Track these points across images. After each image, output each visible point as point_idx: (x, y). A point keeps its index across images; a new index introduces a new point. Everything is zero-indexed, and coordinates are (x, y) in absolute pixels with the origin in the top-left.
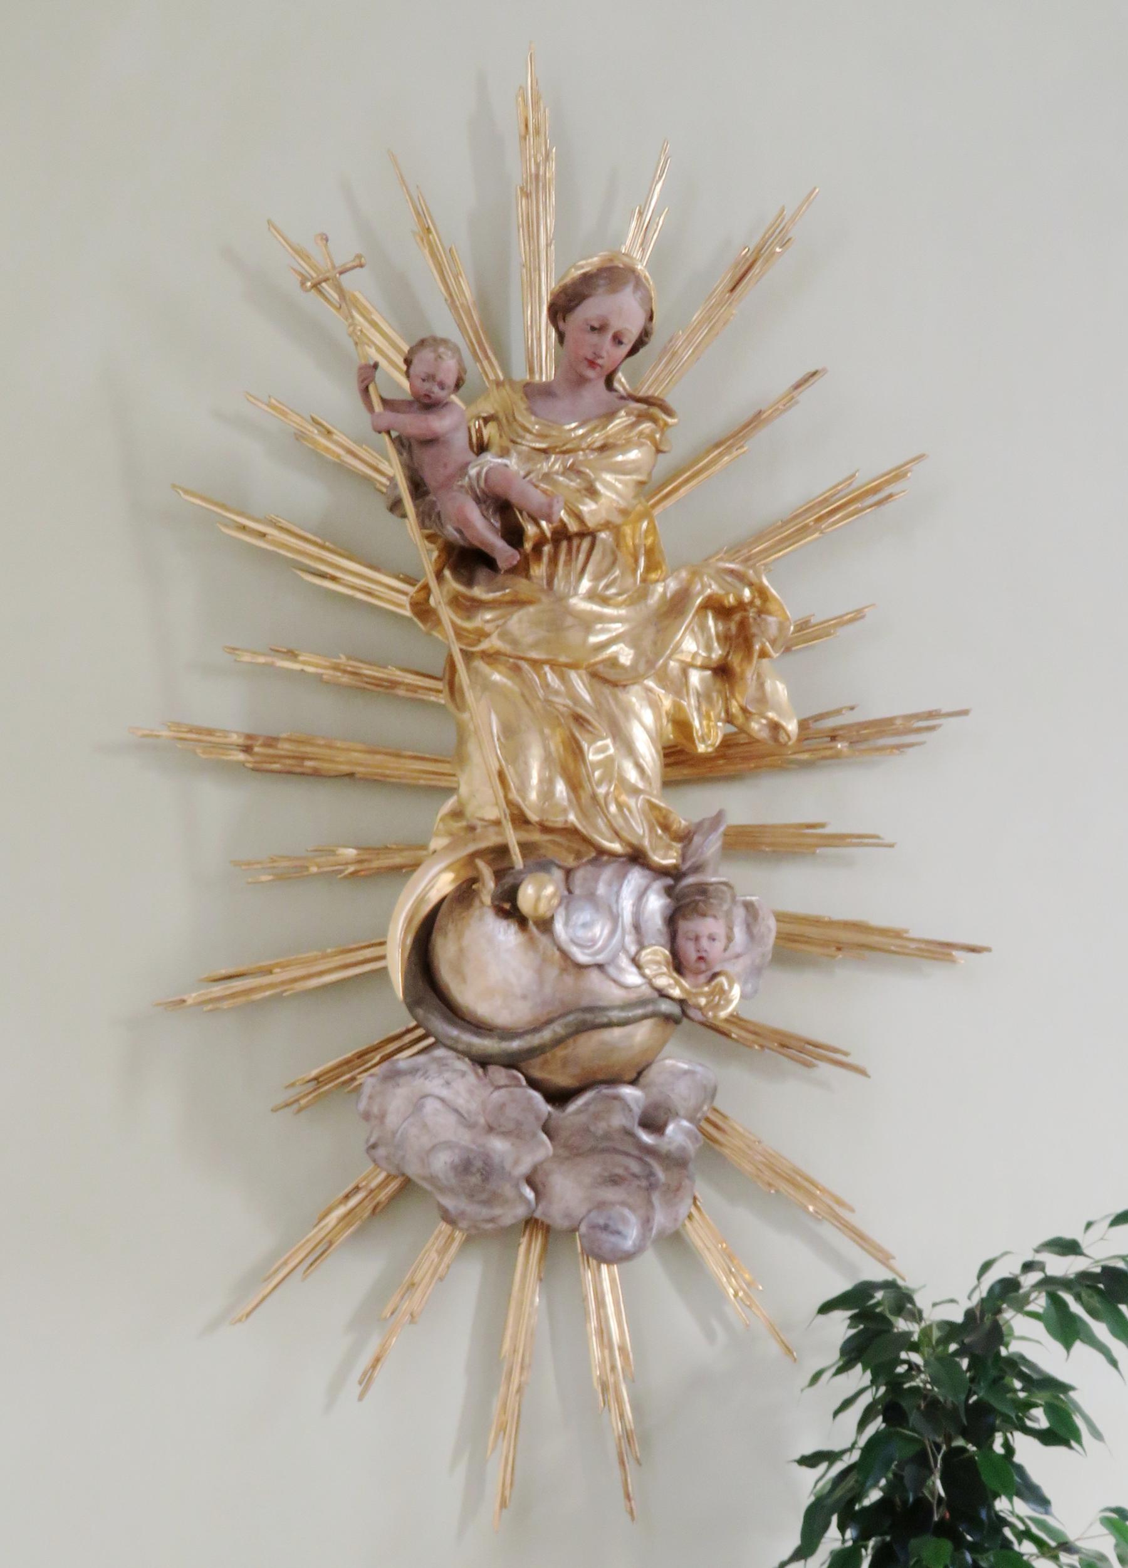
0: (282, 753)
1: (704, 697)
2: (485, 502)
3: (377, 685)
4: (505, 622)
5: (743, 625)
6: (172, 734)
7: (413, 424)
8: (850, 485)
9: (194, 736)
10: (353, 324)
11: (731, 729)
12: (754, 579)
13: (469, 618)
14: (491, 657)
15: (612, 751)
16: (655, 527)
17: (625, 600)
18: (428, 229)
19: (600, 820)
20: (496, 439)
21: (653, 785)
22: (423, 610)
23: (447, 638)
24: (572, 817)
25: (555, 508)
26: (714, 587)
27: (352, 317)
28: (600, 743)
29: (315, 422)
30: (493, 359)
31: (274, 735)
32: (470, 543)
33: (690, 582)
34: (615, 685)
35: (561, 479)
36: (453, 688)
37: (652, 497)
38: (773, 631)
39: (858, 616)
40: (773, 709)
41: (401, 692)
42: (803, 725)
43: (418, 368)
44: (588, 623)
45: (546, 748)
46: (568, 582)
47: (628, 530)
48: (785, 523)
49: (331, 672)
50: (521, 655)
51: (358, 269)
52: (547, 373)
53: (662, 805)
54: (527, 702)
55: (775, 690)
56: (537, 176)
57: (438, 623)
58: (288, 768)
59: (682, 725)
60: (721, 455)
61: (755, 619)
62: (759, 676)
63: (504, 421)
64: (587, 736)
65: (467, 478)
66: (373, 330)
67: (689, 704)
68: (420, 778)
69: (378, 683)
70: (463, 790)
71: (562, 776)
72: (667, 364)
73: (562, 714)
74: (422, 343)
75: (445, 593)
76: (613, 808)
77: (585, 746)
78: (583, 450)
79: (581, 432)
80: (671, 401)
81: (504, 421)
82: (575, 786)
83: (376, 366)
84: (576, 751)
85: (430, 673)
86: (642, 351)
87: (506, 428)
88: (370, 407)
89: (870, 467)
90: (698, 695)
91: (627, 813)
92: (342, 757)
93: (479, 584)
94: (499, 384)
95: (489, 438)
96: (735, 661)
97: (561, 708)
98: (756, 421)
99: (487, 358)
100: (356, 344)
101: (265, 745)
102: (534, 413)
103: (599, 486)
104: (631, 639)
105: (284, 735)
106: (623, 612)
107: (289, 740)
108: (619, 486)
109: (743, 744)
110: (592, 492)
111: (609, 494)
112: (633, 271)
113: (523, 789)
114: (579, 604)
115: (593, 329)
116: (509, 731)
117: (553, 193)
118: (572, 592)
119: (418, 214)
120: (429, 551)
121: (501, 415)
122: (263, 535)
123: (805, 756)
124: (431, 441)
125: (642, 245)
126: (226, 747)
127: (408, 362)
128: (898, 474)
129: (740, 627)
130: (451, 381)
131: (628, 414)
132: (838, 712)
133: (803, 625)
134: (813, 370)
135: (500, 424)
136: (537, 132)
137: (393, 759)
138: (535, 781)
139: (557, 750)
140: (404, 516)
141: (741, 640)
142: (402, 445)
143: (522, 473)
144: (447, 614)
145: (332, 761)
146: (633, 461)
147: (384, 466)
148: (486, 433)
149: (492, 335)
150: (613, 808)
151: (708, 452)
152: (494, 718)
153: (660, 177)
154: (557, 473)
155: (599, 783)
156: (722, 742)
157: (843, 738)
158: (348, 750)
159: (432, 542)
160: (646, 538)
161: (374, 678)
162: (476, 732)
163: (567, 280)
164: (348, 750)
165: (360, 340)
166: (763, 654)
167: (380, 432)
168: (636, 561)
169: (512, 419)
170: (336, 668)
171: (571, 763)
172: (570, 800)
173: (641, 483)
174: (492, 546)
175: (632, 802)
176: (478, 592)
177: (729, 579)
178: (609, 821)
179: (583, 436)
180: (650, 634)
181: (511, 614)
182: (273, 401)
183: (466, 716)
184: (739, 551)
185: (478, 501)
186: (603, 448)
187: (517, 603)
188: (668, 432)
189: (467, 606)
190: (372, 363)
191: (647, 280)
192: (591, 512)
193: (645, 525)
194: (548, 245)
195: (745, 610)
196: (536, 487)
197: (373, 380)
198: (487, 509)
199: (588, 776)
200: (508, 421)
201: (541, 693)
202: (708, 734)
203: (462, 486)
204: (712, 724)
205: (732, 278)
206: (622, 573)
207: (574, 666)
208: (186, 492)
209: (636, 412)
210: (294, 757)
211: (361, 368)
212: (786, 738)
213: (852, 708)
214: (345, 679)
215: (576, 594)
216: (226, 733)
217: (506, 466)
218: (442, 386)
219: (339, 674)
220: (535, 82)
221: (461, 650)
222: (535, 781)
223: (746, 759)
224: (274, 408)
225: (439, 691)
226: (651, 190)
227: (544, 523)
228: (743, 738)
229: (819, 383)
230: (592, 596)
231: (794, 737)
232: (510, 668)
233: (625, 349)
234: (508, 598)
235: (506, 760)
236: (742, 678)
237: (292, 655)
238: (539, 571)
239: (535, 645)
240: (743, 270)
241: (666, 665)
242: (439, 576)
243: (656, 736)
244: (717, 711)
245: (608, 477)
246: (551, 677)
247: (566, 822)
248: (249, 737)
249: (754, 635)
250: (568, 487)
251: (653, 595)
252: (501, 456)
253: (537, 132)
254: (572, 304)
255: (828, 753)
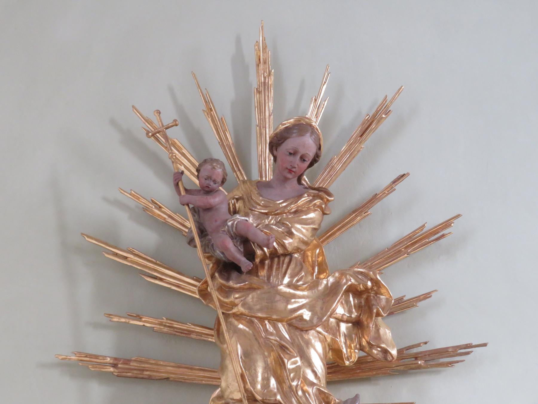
0: (132, 367)
1: (348, 336)
2: (236, 239)
3: (182, 333)
4: (245, 299)
5: (367, 300)
6: (77, 358)
7: (200, 200)
8: (422, 230)
9: (88, 359)
10: (172, 153)
11: (363, 354)
12: (373, 277)
13: (227, 297)
14: (239, 317)
15: (299, 363)
16: (323, 252)
17: (307, 287)
18: (211, 109)
19: (293, 399)
20: (242, 208)
21: (322, 382)
22: (204, 294)
23: (216, 307)
24: (279, 397)
25: (271, 241)
26: (353, 281)
27: (171, 150)
28: (293, 360)
29: (153, 202)
30: (243, 172)
31: (128, 358)
32: (228, 259)
33: (340, 278)
34: (302, 330)
35: (274, 227)
36: (219, 333)
37: (322, 237)
38: (383, 303)
39: (427, 296)
40: (383, 343)
41: (193, 336)
42: (400, 351)
43: (203, 173)
44: (288, 298)
45: (266, 362)
46: (278, 278)
47: (309, 254)
48: (389, 249)
49: (158, 326)
50: (253, 315)
51: (175, 127)
52: (269, 176)
53: (326, 391)
54: (256, 339)
55: (386, 333)
56: (265, 82)
57: (212, 300)
58: (135, 375)
59: (337, 352)
60: (356, 216)
61: (374, 297)
62: (376, 326)
63: (246, 200)
64: (286, 356)
65: (226, 227)
66: (183, 158)
67: (340, 341)
68: (202, 380)
69: (182, 331)
70: (223, 384)
71: (274, 377)
72: (329, 172)
73: (274, 344)
74: (205, 161)
75: (215, 285)
76: (300, 393)
77: (286, 361)
78: (286, 213)
79: (284, 204)
80: (331, 189)
81: (246, 200)
82: (280, 382)
83: (182, 173)
84: (282, 365)
85: (208, 327)
86: (316, 165)
87: (247, 204)
88: (179, 193)
89: (433, 220)
90: (345, 336)
91: (307, 396)
92: (163, 369)
93: (232, 280)
94: (244, 182)
95: (239, 208)
96: (364, 318)
97: (273, 341)
98: (374, 199)
99: (239, 170)
100: (173, 162)
101: (124, 363)
102: (261, 196)
103: (293, 231)
104: (311, 307)
105: (133, 359)
106: (305, 293)
107: (135, 361)
108: (304, 231)
109: (370, 362)
110: (290, 234)
111: (298, 234)
112: (311, 125)
113: (254, 383)
114: (283, 288)
115: (290, 154)
116: (247, 355)
117: (272, 91)
118: (280, 283)
119: (206, 102)
120: (208, 265)
121: (245, 197)
122: (126, 258)
123: (402, 368)
124: (209, 209)
125: (316, 115)
126: (105, 364)
127: (198, 170)
128: (447, 224)
129: (366, 301)
130: (219, 180)
131: (308, 196)
132: (418, 345)
133: (399, 301)
134: (402, 174)
135: (244, 202)
136: (265, 63)
137: (189, 371)
138: (260, 379)
139: (271, 363)
140: (195, 246)
141: (367, 307)
142: (195, 211)
143: (255, 225)
144: (215, 295)
145: (157, 372)
146: (311, 219)
147: (187, 224)
148: (237, 205)
149: (241, 157)
150: (300, 393)
151: (350, 215)
152: (239, 346)
153: (325, 83)
154: (272, 224)
155: (293, 380)
156: (357, 361)
157: (421, 358)
158: (166, 366)
159: (210, 260)
160: (318, 257)
161: (180, 329)
162: (230, 355)
163: (278, 130)
164: (166, 366)
165: (175, 161)
166: (378, 314)
167: (184, 205)
168: (313, 269)
169: (250, 198)
170: (161, 324)
171: (278, 369)
172: (278, 389)
173: (315, 229)
174: (239, 260)
175: (310, 390)
176: (231, 283)
177: (360, 277)
178: (298, 399)
179: (285, 207)
180: (319, 304)
181: (249, 295)
182: (133, 192)
183: (225, 346)
184: (366, 264)
185: (232, 238)
186: (296, 212)
187: (251, 289)
188: (330, 204)
189: (226, 291)
190: (180, 171)
191: (317, 130)
192: (289, 243)
193: (318, 251)
194: (270, 116)
195: (369, 293)
196: (262, 231)
197: (181, 180)
198: (237, 242)
199: (287, 376)
200: (248, 199)
201: (263, 334)
202: (351, 355)
203: (224, 231)
204: (352, 351)
205: (361, 130)
206: (306, 274)
207: (281, 321)
208: (88, 237)
209: (312, 194)
210: (139, 370)
211: (174, 174)
212: (391, 358)
213: (426, 343)
214: (166, 330)
215: (282, 284)
216: (105, 357)
217: (247, 221)
218: (215, 182)
219: (162, 327)
220: (264, 39)
221: (223, 313)
222: (260, 379)
223: (371, 370)
224: (133, 196)
225: (213, 336)
226: (320, 89)
227: (265, 249)
228: (369, 359)
229: (406, 180)
230: (289, 285)
231: (395, 358)
232: (247, 322)
233: (307, 163)
234: (246, 287)
235: (245, 369)
236: (368, 327)
237: (139, 318)
238: (263, 273)
239: (260, 310)
240: (366, 126)
241: (328, 320)
242: (213, 277)
243: (324, 358)
244: (355, 344)
245: (299, 226)
246: (268, 326)
247: (276, 400)
248: (116, 359)
249: (373, 305)
250: (277, 231)
251: (321, 285)
252: (245, 216)
253: (265, 63)
254: (280, 142)
255: (414, 366)
